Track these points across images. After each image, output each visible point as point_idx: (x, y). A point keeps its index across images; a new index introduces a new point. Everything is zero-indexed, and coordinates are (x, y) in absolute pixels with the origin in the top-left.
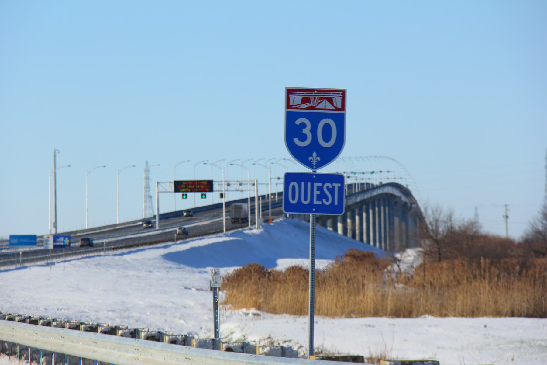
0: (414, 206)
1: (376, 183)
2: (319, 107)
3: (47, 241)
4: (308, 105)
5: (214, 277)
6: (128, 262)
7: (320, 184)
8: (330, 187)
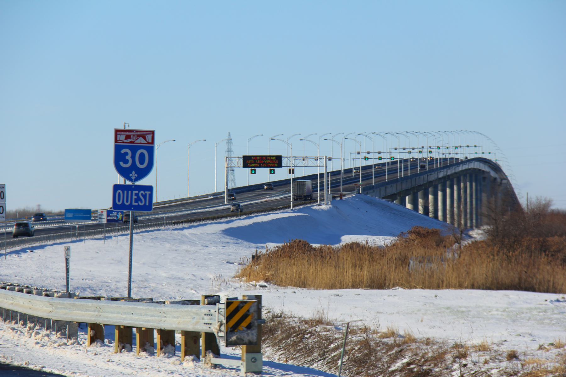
0: (504, 181)
1: (461, 157)
2: (137, 142)
3: (101, 215)
4: (130, 140)
5: (67, 252)
6: (187, 237)
7: (137, 192)
8: (144, 194)
